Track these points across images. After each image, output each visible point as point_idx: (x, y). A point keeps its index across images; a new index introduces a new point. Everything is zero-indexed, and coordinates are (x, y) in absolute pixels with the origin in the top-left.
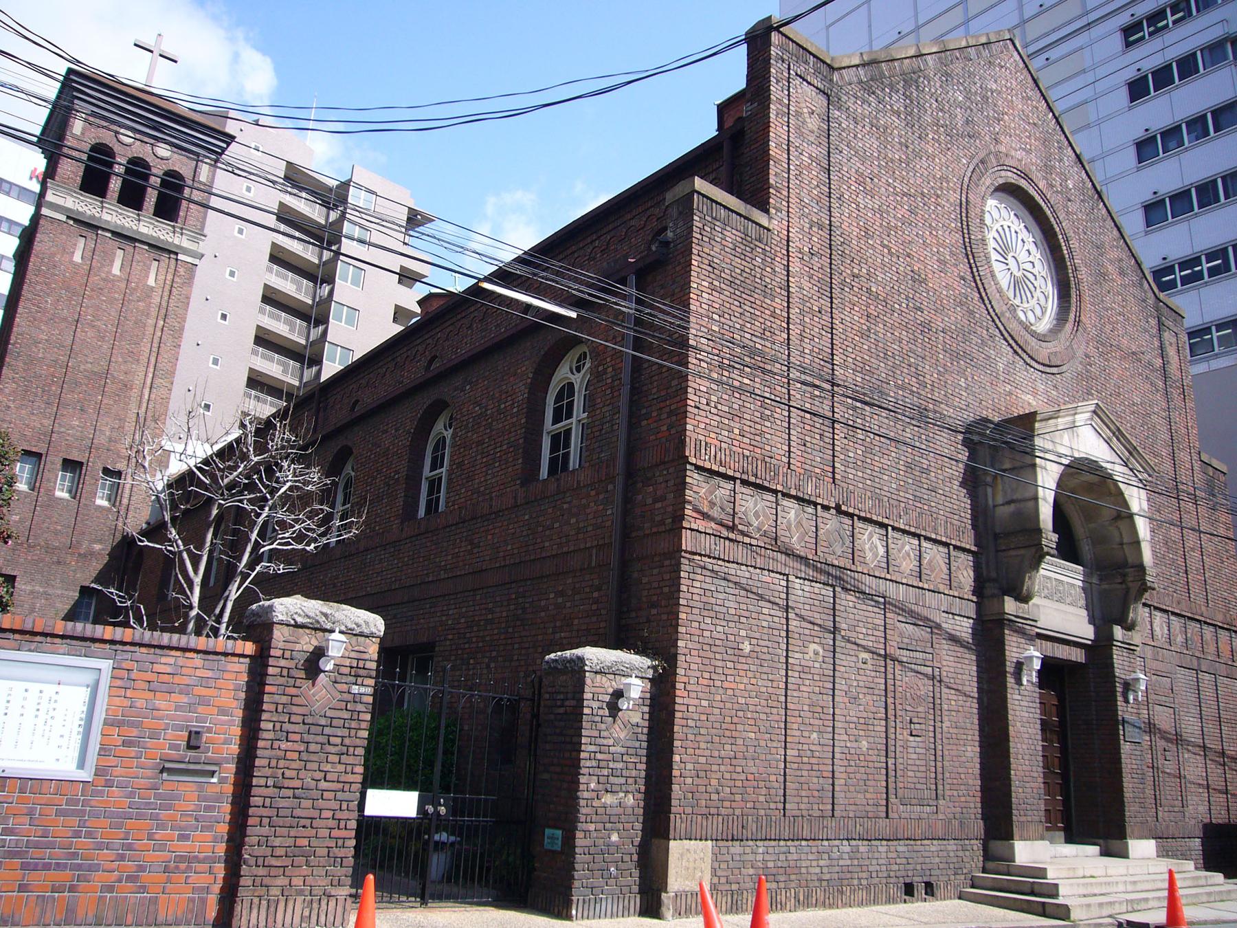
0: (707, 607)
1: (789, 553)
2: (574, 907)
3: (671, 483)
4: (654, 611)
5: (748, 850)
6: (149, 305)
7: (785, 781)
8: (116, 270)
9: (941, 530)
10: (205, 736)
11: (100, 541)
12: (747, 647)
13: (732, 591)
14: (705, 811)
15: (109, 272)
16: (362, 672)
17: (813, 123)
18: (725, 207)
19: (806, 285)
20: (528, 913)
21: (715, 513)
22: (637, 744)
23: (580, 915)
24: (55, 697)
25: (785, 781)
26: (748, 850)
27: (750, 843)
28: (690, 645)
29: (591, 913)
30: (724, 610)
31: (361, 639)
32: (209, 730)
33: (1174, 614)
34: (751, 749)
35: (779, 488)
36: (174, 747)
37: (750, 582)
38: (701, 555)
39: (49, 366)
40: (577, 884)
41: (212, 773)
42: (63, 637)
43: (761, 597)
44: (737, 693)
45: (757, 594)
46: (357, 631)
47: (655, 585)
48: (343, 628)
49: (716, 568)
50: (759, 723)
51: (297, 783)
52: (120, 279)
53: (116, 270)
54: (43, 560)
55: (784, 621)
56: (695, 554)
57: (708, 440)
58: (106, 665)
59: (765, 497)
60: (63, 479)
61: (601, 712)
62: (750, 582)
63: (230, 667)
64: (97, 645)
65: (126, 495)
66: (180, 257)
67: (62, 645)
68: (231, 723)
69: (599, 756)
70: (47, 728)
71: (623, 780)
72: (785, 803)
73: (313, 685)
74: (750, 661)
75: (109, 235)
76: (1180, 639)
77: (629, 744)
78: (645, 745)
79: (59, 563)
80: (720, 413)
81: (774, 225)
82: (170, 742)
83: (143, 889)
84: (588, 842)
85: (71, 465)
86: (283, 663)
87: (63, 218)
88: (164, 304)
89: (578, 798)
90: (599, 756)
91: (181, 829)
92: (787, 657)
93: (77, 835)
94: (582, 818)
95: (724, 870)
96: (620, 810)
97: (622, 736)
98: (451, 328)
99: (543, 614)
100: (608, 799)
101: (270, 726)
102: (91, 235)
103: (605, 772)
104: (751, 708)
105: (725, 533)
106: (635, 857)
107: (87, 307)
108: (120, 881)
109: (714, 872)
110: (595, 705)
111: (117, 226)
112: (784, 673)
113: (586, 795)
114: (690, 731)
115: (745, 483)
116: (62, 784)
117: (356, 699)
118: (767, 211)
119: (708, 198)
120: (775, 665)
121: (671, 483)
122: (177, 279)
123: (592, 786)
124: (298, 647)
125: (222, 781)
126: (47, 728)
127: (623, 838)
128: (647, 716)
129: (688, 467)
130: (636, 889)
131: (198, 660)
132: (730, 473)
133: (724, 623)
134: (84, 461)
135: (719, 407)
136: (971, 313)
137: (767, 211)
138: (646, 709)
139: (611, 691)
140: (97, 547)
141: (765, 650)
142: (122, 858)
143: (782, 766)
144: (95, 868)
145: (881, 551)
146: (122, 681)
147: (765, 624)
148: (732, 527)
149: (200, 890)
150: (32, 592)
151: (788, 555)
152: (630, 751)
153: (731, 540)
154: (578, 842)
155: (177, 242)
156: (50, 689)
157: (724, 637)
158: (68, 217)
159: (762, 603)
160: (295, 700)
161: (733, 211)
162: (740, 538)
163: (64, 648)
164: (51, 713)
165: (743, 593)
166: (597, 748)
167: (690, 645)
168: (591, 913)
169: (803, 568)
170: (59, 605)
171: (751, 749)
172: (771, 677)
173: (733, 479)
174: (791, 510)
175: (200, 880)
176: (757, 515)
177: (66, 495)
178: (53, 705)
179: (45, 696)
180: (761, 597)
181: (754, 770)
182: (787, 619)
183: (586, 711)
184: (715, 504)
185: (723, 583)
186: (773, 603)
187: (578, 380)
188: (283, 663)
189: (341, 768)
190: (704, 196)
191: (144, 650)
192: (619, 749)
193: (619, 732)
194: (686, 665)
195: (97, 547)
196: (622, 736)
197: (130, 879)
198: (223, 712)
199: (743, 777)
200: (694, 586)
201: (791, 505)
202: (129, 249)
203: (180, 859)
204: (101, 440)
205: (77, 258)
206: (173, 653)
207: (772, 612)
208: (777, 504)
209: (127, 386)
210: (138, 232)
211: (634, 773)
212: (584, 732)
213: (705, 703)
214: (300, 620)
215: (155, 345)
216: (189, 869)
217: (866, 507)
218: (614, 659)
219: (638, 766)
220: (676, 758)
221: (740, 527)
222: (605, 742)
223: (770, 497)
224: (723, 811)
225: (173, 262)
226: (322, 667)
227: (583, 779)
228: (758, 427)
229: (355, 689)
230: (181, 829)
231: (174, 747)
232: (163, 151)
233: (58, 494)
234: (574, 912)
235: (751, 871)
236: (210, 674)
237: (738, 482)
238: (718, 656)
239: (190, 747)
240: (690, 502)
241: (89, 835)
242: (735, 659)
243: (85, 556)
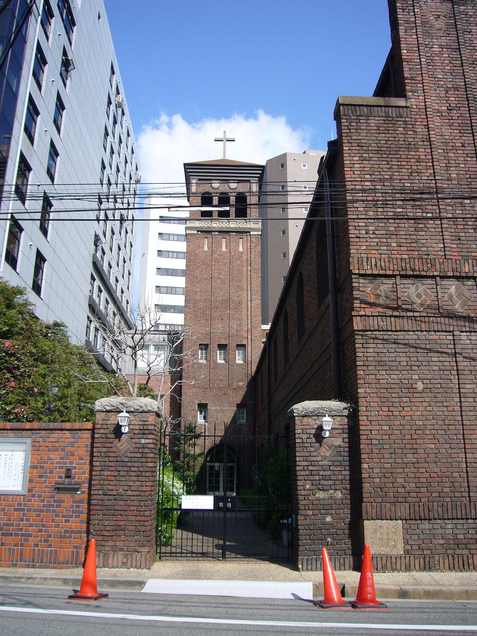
0: (380, 363)
1: (452, 315)
2: (300, 562)
5: (436, 526)
6: (242, 261)
7: (468, 477)
8: (224, 249)
10: (73, 471)
11: (242, 381)
12: (420, 386)
13: (402, 350)
14: (393, 500)
15: (221, 251)
16: (146, 432)
18: (367, 106)
19: (446, 131)
20: (283, 566)
21: (381, 301)
22: (341, 459)
23: (305, 568)
24: (12, 457)
25: (468, 477)
26: (436, 526)
27: (439, 521)
28: (368, 390)
29: (314, 567)
30: (397, 364)
31: (143, 414)
32: (75, 468)
34: (432, 456)
35: (436, 274)
36: (60, 477)
37: (418, 342)
38: (372, 331)
39: (204, 302)
40: (301, 548)
41: (77, 489)
42: (11, 430)
43: (430, 350)
44: (414, 418)
45: (427, 349)
46: (141, 410)
48: (128, 409)
49: (385, 337)
50: (437, 436)
51: (114, 493)
52: (226, 252)
53: (224, 249)
54: (217, 394)
55: (454, 364)
56: (367, 331)
57: (369, 256)
58: (29, 441)
59: (425, 282)
60: (220, 354)
61: (309, 441)
62: (418, 342)
63: (83, 436)
64: (24, 432)
65: (250, 356)
66: (252, 233)
67: (11, 434)
68: (85, 464)
69: (311, 468)
70: (9, 471)
71: (331, 482)
72: (469, 492)
73: (119, 441)
74: (424, 395)
75: (217, 233)
77: (335, 459)
78: (347, 458)
79: (225, 394)
80: (378, 236)
81: (412, 102)
82: (58, 476)
83: (50, 546)
84: (308, 522)
85: (222, 347)
86: (102, 431)
87: (196, 232)
88: (249, 258)
89: (297, 495)
90: (311, 468)
91: (66, 516)
92: (459, 388)
93: (22, 520)
94: (302, 507)
95: (414, 540)
96: (333, 502)
97: (328, 454)
100: (321, 495)
101: (98, 464)
102: (209, 236)
103: (317, 478)
104: (428, 427)
105: (390, 312)
106: (347, 531)
107: (215, 270)
108: (41, 542)
109: (406, 542)
110: (304, 437)
111: (219, 228)
112: (458, 399)
113: (303, 492)
114: (376, 447)
115: (403, 277)
116: (16, 495)
117: (144, 446)
118: (405, 96)
119: (351, 105)
120: (448, 395)
122: (252, 245)
123: (308, 487)
124: (109, 422)
125: (83, 492)
126: (9, 471)
127: (336, 519)
128: (347, 440)
129: (353, 276)
130: (349, 552)
131: (68, 434)
132: (390, 273)
133: (398, 372)
134: (227, 343)
135: (377, 232)
137: (405, 96)
138: (346, 436)
139: (316, 426)
140: (241, 384)
141: (439, 386)
142: (41, 531)
143: (465, 465)
144: (30, 535)
146: (35, 448)
147: (435, 368)
148: (397, 308)
149: (75, 547)
150: (216, 410)
151: (452, 318)
152: (335, 463)
153: (396, 317)
154: (300, 522)
155: (248, 226)
156: (9, 453)
157: (398, 382)
158: (198, 231)
159: (432, 354)
160: (111, 450)
161: (373, 106)
162: (404, 314)
165: (412, 350)
166: (309, 463)
167: (368, 390)
168: (314, 567)
169: (467, 324)
170: (228, 415)
171: (432, 456)
172: (445, 404)
173: (394, 276)
174: (452, 287)
175: (77, 542)
176: (419, 296)
177: (223, 362)
178: (11, 461)
179: (8, 457)
180: (430, 350)
181: (436, 470)
182: (456, 362)
183: (297, 441)
184: (380, 296)
185: (393, 346)
186: (442, 353)
188: (102, 431)
189: (138, 483)
190: (347, 105)
191: (44, 432)
192: (326, 463)
193: (325, 452)
194: (366, 404)
195: (241, 384)
196: (328, 454)
197: (46, 541)
198: (81, 459)
199: (427, 475)
200: (366, 352)
201: (451, 283)
202: (228, 237)
203: (66, 532)
204: (233, 332)
205: (206, 249)
206: (57, 432)
207: (442, 359)
208: (437, 285)
209: (240, 303)
210: (229, 227)
211: (340, 477)
212: (297, 454)
214: (108, 408)
215: (249, 279)
216: (70, 537)
218: (316, 406)
219: (343, 473)
220: (365, 466)
221: (404, 306)
222: (315, 459)
223: (430, 281)
224: (410, 500)
225: (249, 236)
226: (123, 431)
227: (299, 483)
228: (414, 237)
229: (143, 441)
230: (66, 516)
231: (60, 477)
232: (233, 185)
233: (219, 361)
234: (300, 566)
235: (442, 541)
237: (398, 277)
238: (394, 395)
239: (68, 477)
240: (357, 299)
241: (27, 520)
242: (411, 395)
243: (236, 389)
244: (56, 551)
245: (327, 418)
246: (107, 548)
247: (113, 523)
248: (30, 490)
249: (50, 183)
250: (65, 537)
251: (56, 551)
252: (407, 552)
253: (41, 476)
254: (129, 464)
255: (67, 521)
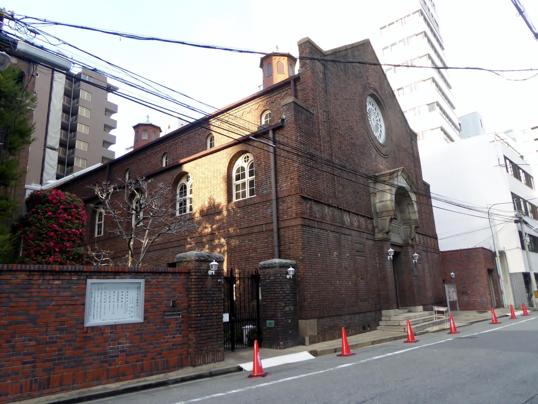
3: (294, 202)
4: (291, 245)
9: (363, 212)
17: (321, 75)
33: (421, 234)
47: (291, 236)
58: (142, 281)
76: (422, 242)
98: (173, 142)
99: (243, 248)
116: (134, 325)
121: (294, 202)
136: (365, 139)
145: (349, 220)
163: (129, 276)
164: (127, 300)
187: (246, 166)
213: (311, 274)
216: (176, 348)
217: (344, 206)
236: (174, 280)
244: (167, 361)
245: (291, 269)
246: (204, 352)
247: (206, 334)
248: (145, 318)
249: (402, 90)
250: (173, 349)
251: (167, 361)
252: (318, 334)
253: (153, 308)
254: (213, 295)
255: (173, 338)
